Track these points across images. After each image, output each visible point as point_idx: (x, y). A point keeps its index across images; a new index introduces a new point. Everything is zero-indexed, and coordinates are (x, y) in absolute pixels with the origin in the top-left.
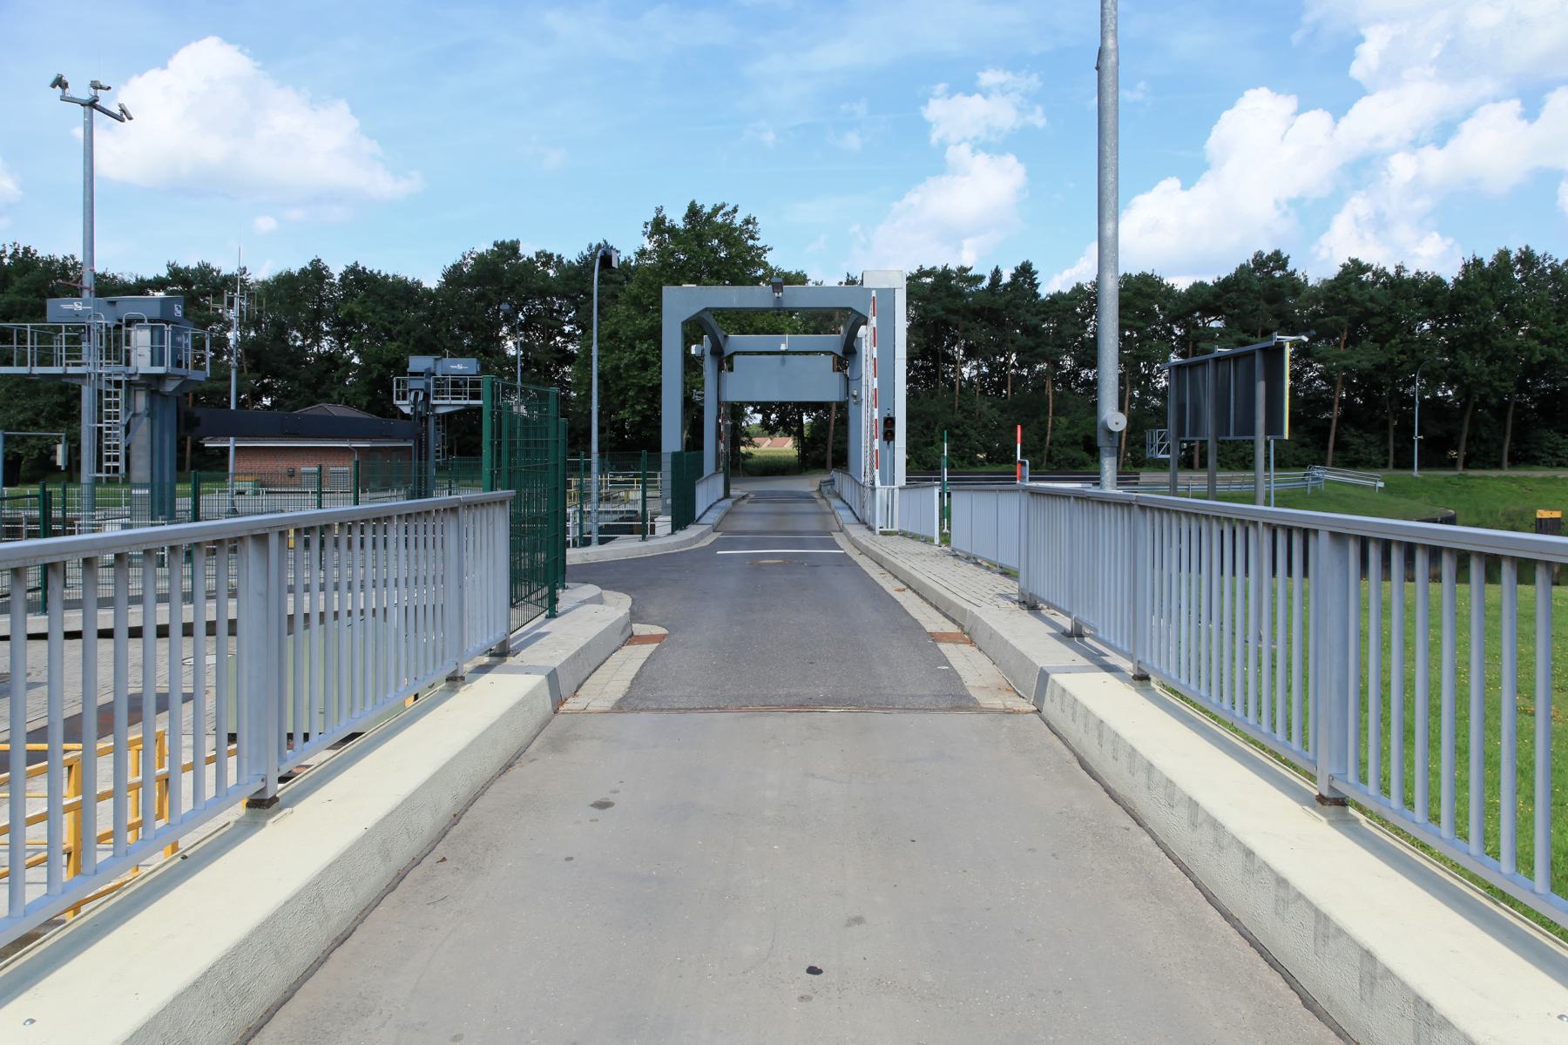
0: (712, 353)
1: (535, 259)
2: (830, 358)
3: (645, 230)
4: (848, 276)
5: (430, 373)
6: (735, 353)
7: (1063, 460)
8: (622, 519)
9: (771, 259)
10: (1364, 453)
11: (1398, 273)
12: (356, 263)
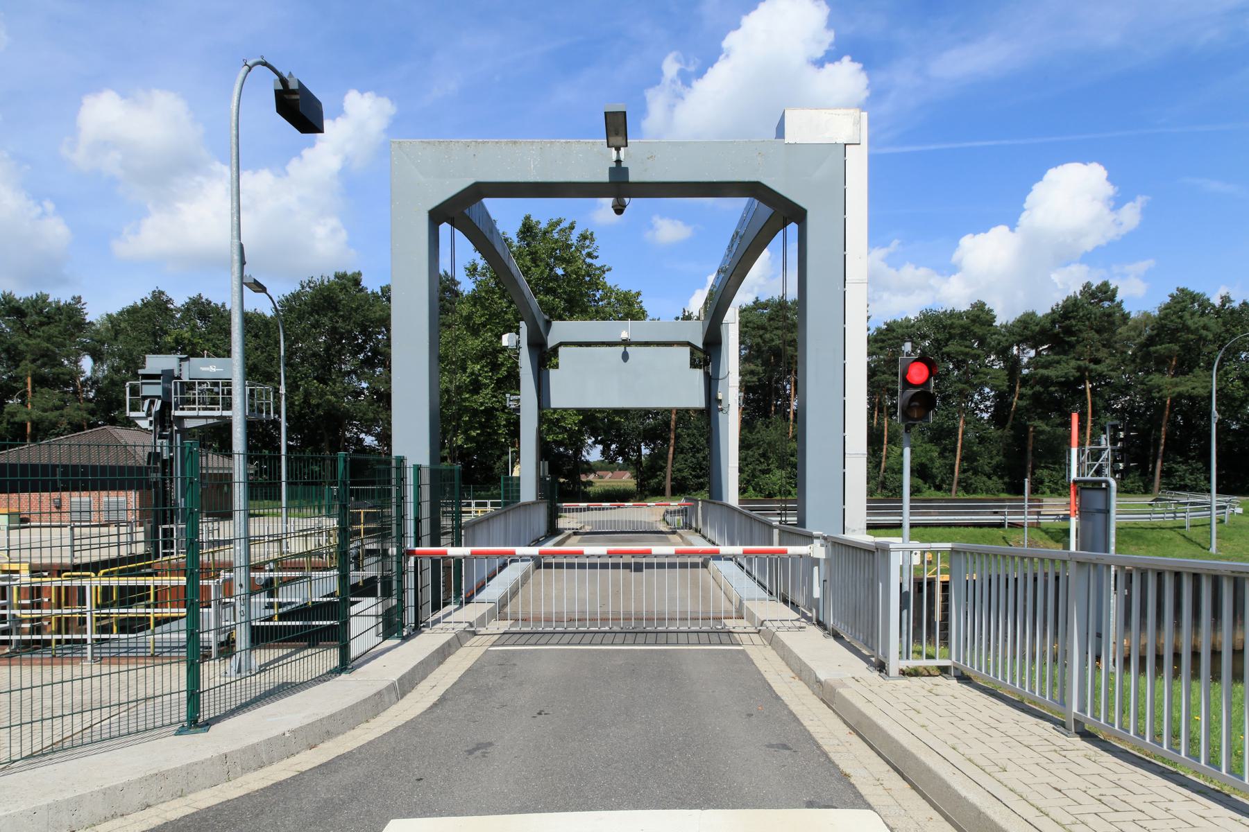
0: (531, 345)
1: (380, 294)
2: (687, 350)
4: (684, 311)
5: (168, 376)
6: (561, 344)
8: (282, 617)
9: (610, 280)
11: (1223, 305)
12: (200, 294)
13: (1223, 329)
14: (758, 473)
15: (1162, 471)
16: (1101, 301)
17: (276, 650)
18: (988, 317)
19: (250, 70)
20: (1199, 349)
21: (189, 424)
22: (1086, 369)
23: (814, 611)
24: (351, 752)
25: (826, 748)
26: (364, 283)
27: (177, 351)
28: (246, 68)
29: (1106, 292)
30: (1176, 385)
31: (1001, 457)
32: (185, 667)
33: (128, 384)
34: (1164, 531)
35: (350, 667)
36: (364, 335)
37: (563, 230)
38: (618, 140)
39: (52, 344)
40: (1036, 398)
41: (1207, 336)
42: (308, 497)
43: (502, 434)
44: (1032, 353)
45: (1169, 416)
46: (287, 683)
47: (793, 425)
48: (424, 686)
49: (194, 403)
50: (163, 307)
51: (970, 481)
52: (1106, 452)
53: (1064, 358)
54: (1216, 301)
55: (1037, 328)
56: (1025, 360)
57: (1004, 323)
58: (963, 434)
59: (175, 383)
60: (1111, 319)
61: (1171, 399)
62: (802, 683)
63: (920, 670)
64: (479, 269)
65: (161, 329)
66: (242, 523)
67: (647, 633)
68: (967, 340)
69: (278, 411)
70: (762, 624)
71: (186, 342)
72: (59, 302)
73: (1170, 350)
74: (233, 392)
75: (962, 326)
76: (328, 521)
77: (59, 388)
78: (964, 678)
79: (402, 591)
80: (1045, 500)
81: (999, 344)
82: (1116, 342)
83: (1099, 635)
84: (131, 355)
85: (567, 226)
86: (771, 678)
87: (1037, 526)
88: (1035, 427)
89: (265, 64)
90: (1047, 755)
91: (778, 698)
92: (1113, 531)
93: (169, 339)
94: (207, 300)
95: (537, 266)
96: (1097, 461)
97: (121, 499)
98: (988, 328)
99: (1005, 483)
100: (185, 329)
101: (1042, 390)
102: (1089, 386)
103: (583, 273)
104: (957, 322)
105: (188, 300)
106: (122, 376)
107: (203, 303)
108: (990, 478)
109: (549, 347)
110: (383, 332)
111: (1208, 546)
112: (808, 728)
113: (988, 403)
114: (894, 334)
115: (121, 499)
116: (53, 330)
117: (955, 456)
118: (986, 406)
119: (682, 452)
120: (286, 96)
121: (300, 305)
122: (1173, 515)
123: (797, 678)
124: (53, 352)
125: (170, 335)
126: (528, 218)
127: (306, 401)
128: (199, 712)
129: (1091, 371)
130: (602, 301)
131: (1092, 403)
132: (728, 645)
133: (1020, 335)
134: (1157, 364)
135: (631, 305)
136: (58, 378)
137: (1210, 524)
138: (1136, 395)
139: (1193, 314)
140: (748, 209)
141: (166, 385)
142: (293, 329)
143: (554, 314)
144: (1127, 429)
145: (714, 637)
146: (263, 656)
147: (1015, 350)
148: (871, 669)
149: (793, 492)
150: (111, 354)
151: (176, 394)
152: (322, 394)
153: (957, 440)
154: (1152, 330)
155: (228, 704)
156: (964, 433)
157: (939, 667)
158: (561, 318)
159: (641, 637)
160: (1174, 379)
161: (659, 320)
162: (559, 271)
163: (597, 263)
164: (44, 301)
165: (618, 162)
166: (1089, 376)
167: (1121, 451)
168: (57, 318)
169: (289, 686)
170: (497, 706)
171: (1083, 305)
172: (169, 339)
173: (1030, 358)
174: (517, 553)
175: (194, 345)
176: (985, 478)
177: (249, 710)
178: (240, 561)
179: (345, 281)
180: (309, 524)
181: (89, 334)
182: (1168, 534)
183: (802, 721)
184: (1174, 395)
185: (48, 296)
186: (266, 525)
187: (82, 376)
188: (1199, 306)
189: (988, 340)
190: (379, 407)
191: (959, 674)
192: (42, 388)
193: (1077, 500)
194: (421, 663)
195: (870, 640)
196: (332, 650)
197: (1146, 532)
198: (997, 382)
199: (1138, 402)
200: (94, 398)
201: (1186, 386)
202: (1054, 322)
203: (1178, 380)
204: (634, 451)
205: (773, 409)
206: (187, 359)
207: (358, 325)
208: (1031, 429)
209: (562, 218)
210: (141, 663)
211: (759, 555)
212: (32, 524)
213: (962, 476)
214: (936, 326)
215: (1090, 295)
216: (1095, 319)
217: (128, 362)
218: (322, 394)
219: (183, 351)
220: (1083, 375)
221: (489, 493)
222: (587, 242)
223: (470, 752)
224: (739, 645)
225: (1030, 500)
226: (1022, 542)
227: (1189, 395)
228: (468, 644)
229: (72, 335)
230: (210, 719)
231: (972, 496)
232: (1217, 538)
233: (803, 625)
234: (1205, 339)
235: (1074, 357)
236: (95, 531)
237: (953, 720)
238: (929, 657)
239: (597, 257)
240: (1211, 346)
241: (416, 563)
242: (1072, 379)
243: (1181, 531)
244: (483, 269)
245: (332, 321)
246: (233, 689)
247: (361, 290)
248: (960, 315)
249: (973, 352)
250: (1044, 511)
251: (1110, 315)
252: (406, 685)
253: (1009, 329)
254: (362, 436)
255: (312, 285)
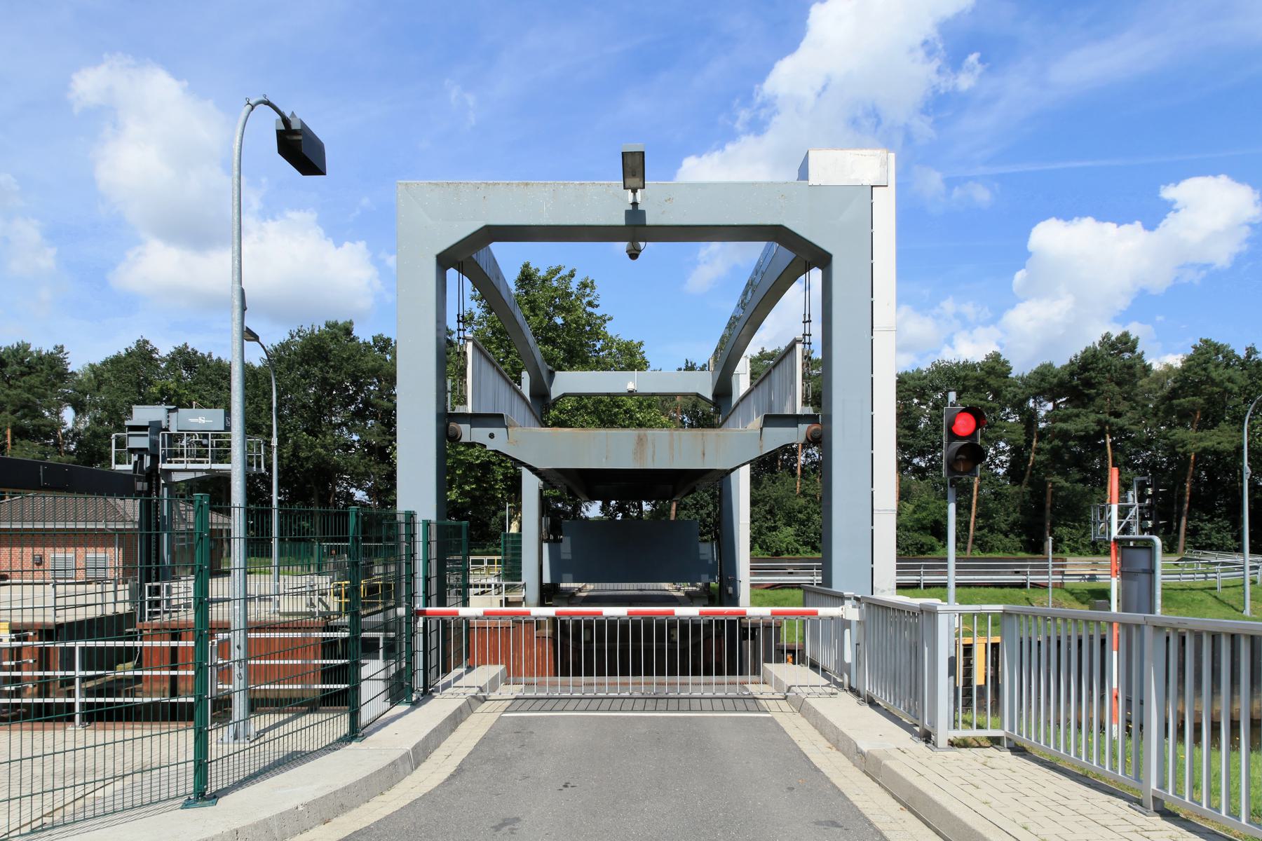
1: (372, 343)
3: (473, 293)
4: (687, 362)
5: (156, 427)
7: (911, 545)
9: (611, 329)
10: (1216, 538)
11: (1249, 357)
12: (186, 344)
13: (1249, 381)
14: (764, 531)
15: (1187, 529)
16: (1121, 352)
17: (272, 716)
18: (1004, 369)
19: (252, 109)
20: (1224, 402)
21: (176, 477)
22: (1107, 422)
23: (846, 676)
24: (368, 827)
25: (879, 826)
26: (355, 333)
27: (162, 402)
28: (249, 107)
29: (1126, 343)
30: (1201, 440)
31: (1018, 515)
32: (193, 734)
33: (113, 435)
34: (1193, 592)
35: (361, 735)
36: (355, 386)
37: (563, 278)
38: (633, 182)
39: (33, 394)
40: (1055, 453)
41: (1232, 389)
42: (295, 553)
43: (499, 489)
44: (1050, 406)
45: (1193, 473)
46: (297, 752)
47: (800, 481)
48: (438, 755)
49: (182, 455)
50: (147, 357)
51: (986, 539)
52: (1134, 509)
53: (1084, 411)
54: (1242, 354)
55: (1055, 381)
56: (1043, 413)
57: (1020, 375)
58: (978, 490)
59: (163, 435)
60: (1132, 371)
61: (1196, 454)
62: (839, 754)
63: (970, 740)
64: (476, 318)
65: (146, 379)
66: (242, 581)
67: (668, 698)
68: (981, 392)
69: (269, 468)
70: (789, 689)
71: (172, 392)
72: (40, 351)
73: (1194, 403)
74: (232, 444)
75: (977, 378)
76: (320, 579)
77: (40, 441)
78: (1018, 750)
79: (412, 654)
80: (1068, 559)
81: (1015, 396)
82: (1137, 395)
83: (1142, 703)
84: (114, 406)
85: (567, 273)
86: (806, 747)
87: (1060, 586)
88: (1054, 483)
89: (268, 103)
90: (1126, 835)
91: (817, 770)
92: (1158, 593)
93: (154, 390)
94: (193, 349)
95: (536, 315)
96: (1124, 518)
97: (69, 555)
98: (1004, 380)
99: (1022, 541)
100: (170, 380)
101: (1060, 444)
102: (1109, 440)
103: (583, 322)
104: (971, 374)
105: (173, 350)
106: (104, 427)
107: (189, 352)
108: (1007, 536)
109: (553, 397)
110: (375, 383)
111: (1241, 608)
112: (855, 803)
113: (1003, 458)
114: (906, 386)
115: (69, 555)
116: (34, 380)
117: (970, 513)
118: (1001, 461)
119: (685, 508)
120: (288, 137)
121: (289, 355)
122: (1204, 576)
123: (834, 749)
124: (34, 403)
125: (155, 386)
126: (526, 266)
127: (295, 454)
128: (207, 784)
129: (1111, 425)
130: (603, 351)
131: (1112, 458)
132: (744, 711)
133: (1037, 388)
134: (1180, 417)
135: (632, 355)
136: (39, 430)
137: (1243, 585)
138: (1158, 449)
139: (1217, 366)
140: (765, 254)
141: (154, 437)
142: (282, 380)
143: (556, 366)
144: (1155, 486)
145: (739, 703)
146: (262, 721)
147: (1031, 404)
148: (916, 739)
149: (801, 551)
150: (93, 405)
151: (163, 446)
152: (312, 447)
153: (972, 496)
154: (1175, 383)
155: (236, 775)
156: (979, 489)
157: (989, 738)
158: (560, 369)
159: (662, 704)
160: (1199, 434)
161: (660, 370)
162: (559, 320)
163: (597, 312)
164: (26, 351)
165: (635, 204)
166: (1110, 430)
167: (1150, 508)
168: (38, 368)
169: (299, 756)
170: (519, 777)
171: (1102, 356)
172: (154, 390)
173: (1048, 411)
174: (532, 614)
175: (180, 396)
176: (1001, 536)
177: (258, 782)
178: (237, 623)
179: (336, 330)
180: (299, 582)
181: (71, 384)
182: (1199, 596)
183: (848, 796)
184: (1199, 450)
185: (29, 345)
186: (258, 583)
187: (63, 428)
188: (1224, 357)
189: (1004, 392)
190: (370, 460)
191: (1013, 745)
192: (22, 440)
193: (1118, 559)
194: (434, 730)
195: (916, 708)
196: (262, 716)
197: (1175, 593)
198: (1014, 437)
199: (1161, 458)
200: (75, 450)
201: (1211, 440)
202: (1072, 374)
203: (1203, 434)
204: (634, 506)
205: (779, 464)
206: (175, 410)
207: (349, 375)
208: (1050, 486)
209: (562, 265)
210: (164, 729)
211: (789, 617)
212: (13, 581)
213: (978, 534)
214: (949, 378)
215: (1110, 346)
216: (1116, 371)
217: (110, 413)
218: (312, 447)
219: (168, 402)
220: (1103, 429)
221: (485, 550)
222: (588, 290)
223: (497, 828)
224: (766, 712)
225: (1054, 559)
226: (1046, 603)
227: (1215, 450)
228: (479, 709)
229: (54, 385)
230: (217, 791)
231: (988, 555)
232: (1251, 600)
233: (835, 691)
234: (1230, 392)
235: (1094, 410)
236: (81, 588)
237: (1017, 796)
238: (979, 727)
239: (597, 306)
240: (1236, 399)
241: (425, 624)
242: (1092, 433)
243: (1213, 592)
244: (479, 317)
245: (322, 371)
246: (242, 758)
247: (353, 340)
248: (973, 367)
249: (988, 405)
250: (1068, 570)
251: (1130, 367)
252: (420, 753)
253: (1026, 381)
254: (353, 490)
255: (301, 334)
